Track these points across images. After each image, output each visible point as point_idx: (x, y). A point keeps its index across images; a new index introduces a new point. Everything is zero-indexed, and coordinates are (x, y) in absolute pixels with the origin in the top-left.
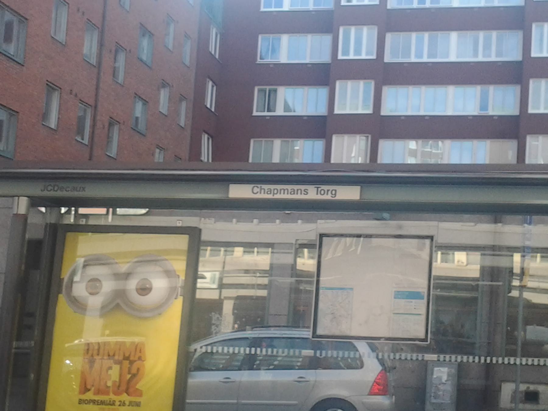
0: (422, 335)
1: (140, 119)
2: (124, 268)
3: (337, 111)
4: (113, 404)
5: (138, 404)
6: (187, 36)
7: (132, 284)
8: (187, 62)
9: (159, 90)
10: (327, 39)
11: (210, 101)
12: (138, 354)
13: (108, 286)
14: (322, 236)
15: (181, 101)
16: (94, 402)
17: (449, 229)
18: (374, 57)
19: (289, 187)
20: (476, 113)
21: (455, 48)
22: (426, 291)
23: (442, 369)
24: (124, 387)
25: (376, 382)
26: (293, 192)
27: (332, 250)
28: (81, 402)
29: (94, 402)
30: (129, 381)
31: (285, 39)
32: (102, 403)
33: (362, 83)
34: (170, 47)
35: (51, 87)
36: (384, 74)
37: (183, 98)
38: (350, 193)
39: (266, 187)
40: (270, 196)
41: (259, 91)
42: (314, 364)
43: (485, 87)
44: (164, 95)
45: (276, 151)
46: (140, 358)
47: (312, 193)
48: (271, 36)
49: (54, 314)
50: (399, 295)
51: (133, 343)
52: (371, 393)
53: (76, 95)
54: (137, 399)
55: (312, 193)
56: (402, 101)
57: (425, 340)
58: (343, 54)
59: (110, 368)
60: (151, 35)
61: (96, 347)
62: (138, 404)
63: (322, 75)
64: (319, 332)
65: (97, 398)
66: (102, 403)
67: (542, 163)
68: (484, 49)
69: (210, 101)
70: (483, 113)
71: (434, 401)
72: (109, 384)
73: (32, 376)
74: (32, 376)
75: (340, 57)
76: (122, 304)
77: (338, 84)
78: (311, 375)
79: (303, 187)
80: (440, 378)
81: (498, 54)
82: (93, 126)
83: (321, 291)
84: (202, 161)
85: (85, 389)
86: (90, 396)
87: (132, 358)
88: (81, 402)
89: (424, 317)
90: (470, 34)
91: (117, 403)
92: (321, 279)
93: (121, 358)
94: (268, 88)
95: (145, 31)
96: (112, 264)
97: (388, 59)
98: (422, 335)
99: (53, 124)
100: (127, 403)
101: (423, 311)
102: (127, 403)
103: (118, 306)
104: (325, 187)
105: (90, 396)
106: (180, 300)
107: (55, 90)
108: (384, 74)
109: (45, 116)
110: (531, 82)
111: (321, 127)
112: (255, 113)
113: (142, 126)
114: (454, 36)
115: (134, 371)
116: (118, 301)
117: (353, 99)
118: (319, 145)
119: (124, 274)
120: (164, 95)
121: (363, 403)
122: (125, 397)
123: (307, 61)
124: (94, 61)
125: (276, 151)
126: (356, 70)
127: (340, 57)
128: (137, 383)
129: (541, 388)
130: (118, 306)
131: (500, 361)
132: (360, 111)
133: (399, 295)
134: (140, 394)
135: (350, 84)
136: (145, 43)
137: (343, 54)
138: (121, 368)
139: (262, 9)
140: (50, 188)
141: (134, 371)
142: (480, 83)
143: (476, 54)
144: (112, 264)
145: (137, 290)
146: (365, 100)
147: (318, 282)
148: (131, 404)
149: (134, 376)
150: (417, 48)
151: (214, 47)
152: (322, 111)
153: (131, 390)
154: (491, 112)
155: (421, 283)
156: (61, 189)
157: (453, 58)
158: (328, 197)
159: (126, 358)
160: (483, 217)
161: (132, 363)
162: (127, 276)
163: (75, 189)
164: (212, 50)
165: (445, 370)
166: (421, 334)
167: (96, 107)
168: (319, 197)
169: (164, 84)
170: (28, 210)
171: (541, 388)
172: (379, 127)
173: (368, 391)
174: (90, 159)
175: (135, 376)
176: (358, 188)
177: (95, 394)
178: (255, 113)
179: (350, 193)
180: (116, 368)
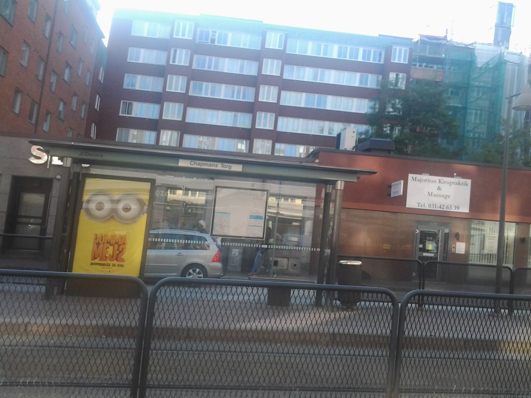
0: (261, 236)
1: (61, 112)
2: (116, 197)
3: (164, 118)
4: (109, 265)
5: (122, 266)
6: (88, 70)
7: (121, 206)
8: (87, 83)
9: (72, 97)
10: (161, 80)
11: (97, 106)
12: (123, 241)
13: (107, 206)
14: (217, 187)
15: (82, 104)
16: (99, 264)
17: (287, 188)
18: (184, 92)
19: (209, 163)
20: (231, 126)
21: (223, 92)
22: (264, 215)
23: (236, 250)
24: (115, 257)
25: (216, 256)
26: (211, 165)
27: (222, 194)
28: (92, 264)
29: (99, 264)
30: (118, 254)
31: (139, 77)
32: (103, 265)
33: (177, 104)
34: (80, 75)
35: (18, 91)
36: (189, 101)
37: (83, 103)
38: (237, 168)
39: (197, 162)
40: (199, 167)
41: (123, 103)
42: (186, 247)
43: (236, 113)
44: (75, 100)
45: (135, 136)
46: (124, 243)
47: (219, 167)
48: (132, 75)
49: (78, 220)
50: (252, 217)
51: (120, 235)
52: (213, 261)
53: (30, 96)
54: (122, 263)
55: (219, 167)
56: (197, 116)
57: (263, 238)
58: (169, 89)
59: (108, 248)
60: (71, 68)
61: (101, 237)
62: (122, 266)
63: (158, 98)
64: (214, 233)
65: (100, 262)
66: (103, 265)
67: (261, 153)
68: (237, 95)
69: (97, 106)
70: (234, 126)
71: (231, 264)
72: (107, 255)
73: (65, 250)
74: (65, 250)
75: (167, 90)
76: (115, 217)
77: (165, 103)
78: (184, 252)
79: (215, 163)
80: (235, 254)
81: (244, 97)
82: (38, 114)
83: (215, 214)
84: (91, 138)
85: (94, 258)
86: (97, 261)
87: (119, 243)
88: (92, 264)
89: (262, 228)
90: (231, 86)
91: (111, 265)
92: (216, 208)
93: (114, 243)
94: (128, 102)
95: (68, 65)
96: (108, 195)
97: (190, 94)
98: (261, 236)
99: (17, 111)
100: (116, 265)
101: (263, 225)
102: (116, 265)
103: (112, 217)
104: (226, 164)
105: (97, 261)
106: (145, 216)
107: (19, 92)
108: (189, 101)
109: (13, 105)
110: (258, 113)
111: (156, 125)
112: (120, 114)
113: (62, 116)
114: (223, 86)
115: (120, 249)
116: (113, 214)
117: (172, 112)
118: (153, 134)
119: (116, 200)
120: (75, 100)
121: (209, 266)
122: (115, 262)
123: (150, 90)
124: (40, 78)
125: (135, 136)
126: (175, 98)
127: (167, 90)
128: (123, 255)
129: (279, 259)
130: (112, 217)
131: (159, 240)
132: (175, 119)
133: (252, 217)
134: (123, 260)
135: (171, 104)
136: (67, 71)
137: (169, 89)
138: (114, 248)
139: (128, 61)
140: (84, 154)
141: (120, 249)
142: (234, 111)
143: (233, 97)
144: (108, 195)
145: (123, 209)
146: (178, 114)
147: (214, 209)
148: (118, 265)
149: (120, 252)
150: (206, 91)
151: (101, 78)
152: (156, 116)
153: (118, 259)
154: (238, 126)
155: (262, 213)
156: (90, 155)
157: (222, 97)
158: (227, 169)
159: (117, 243)
160: (258, 180)
161: (119, 246)
162: (118, 201)
163: (96, 156)
164: (100, 78)
165: (237, 250)
166: (261, 235)
167: (40, 105)
168: (223, 169)
169: (75, 95)
170: (71, 165)
171: (279, 259)
172: (184, 128)
173: (211, 260)
174: (35, 132)
175: (121, 252)
176: (241, 166)
177: (99, 260)
178: (120, 114)
179: (237, 168)
180: (111, 248)
